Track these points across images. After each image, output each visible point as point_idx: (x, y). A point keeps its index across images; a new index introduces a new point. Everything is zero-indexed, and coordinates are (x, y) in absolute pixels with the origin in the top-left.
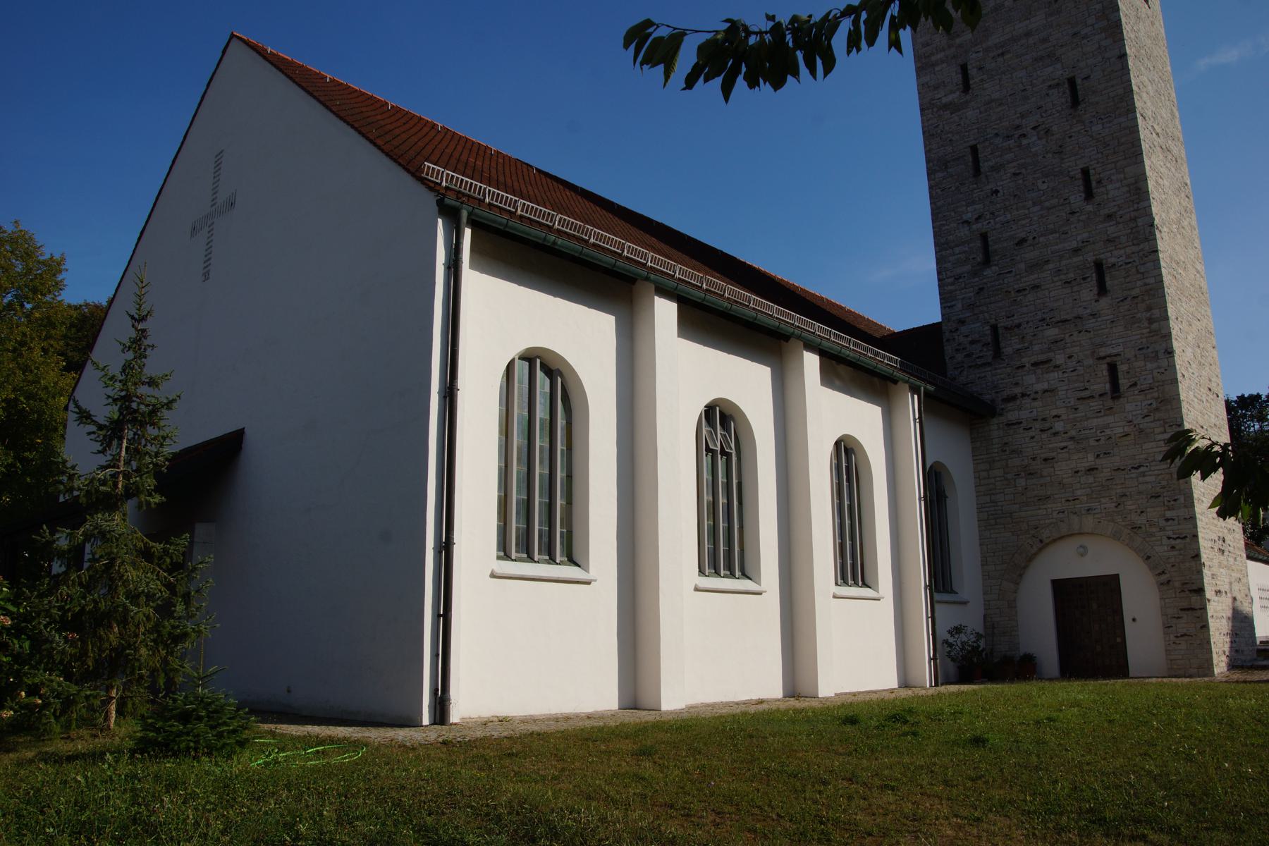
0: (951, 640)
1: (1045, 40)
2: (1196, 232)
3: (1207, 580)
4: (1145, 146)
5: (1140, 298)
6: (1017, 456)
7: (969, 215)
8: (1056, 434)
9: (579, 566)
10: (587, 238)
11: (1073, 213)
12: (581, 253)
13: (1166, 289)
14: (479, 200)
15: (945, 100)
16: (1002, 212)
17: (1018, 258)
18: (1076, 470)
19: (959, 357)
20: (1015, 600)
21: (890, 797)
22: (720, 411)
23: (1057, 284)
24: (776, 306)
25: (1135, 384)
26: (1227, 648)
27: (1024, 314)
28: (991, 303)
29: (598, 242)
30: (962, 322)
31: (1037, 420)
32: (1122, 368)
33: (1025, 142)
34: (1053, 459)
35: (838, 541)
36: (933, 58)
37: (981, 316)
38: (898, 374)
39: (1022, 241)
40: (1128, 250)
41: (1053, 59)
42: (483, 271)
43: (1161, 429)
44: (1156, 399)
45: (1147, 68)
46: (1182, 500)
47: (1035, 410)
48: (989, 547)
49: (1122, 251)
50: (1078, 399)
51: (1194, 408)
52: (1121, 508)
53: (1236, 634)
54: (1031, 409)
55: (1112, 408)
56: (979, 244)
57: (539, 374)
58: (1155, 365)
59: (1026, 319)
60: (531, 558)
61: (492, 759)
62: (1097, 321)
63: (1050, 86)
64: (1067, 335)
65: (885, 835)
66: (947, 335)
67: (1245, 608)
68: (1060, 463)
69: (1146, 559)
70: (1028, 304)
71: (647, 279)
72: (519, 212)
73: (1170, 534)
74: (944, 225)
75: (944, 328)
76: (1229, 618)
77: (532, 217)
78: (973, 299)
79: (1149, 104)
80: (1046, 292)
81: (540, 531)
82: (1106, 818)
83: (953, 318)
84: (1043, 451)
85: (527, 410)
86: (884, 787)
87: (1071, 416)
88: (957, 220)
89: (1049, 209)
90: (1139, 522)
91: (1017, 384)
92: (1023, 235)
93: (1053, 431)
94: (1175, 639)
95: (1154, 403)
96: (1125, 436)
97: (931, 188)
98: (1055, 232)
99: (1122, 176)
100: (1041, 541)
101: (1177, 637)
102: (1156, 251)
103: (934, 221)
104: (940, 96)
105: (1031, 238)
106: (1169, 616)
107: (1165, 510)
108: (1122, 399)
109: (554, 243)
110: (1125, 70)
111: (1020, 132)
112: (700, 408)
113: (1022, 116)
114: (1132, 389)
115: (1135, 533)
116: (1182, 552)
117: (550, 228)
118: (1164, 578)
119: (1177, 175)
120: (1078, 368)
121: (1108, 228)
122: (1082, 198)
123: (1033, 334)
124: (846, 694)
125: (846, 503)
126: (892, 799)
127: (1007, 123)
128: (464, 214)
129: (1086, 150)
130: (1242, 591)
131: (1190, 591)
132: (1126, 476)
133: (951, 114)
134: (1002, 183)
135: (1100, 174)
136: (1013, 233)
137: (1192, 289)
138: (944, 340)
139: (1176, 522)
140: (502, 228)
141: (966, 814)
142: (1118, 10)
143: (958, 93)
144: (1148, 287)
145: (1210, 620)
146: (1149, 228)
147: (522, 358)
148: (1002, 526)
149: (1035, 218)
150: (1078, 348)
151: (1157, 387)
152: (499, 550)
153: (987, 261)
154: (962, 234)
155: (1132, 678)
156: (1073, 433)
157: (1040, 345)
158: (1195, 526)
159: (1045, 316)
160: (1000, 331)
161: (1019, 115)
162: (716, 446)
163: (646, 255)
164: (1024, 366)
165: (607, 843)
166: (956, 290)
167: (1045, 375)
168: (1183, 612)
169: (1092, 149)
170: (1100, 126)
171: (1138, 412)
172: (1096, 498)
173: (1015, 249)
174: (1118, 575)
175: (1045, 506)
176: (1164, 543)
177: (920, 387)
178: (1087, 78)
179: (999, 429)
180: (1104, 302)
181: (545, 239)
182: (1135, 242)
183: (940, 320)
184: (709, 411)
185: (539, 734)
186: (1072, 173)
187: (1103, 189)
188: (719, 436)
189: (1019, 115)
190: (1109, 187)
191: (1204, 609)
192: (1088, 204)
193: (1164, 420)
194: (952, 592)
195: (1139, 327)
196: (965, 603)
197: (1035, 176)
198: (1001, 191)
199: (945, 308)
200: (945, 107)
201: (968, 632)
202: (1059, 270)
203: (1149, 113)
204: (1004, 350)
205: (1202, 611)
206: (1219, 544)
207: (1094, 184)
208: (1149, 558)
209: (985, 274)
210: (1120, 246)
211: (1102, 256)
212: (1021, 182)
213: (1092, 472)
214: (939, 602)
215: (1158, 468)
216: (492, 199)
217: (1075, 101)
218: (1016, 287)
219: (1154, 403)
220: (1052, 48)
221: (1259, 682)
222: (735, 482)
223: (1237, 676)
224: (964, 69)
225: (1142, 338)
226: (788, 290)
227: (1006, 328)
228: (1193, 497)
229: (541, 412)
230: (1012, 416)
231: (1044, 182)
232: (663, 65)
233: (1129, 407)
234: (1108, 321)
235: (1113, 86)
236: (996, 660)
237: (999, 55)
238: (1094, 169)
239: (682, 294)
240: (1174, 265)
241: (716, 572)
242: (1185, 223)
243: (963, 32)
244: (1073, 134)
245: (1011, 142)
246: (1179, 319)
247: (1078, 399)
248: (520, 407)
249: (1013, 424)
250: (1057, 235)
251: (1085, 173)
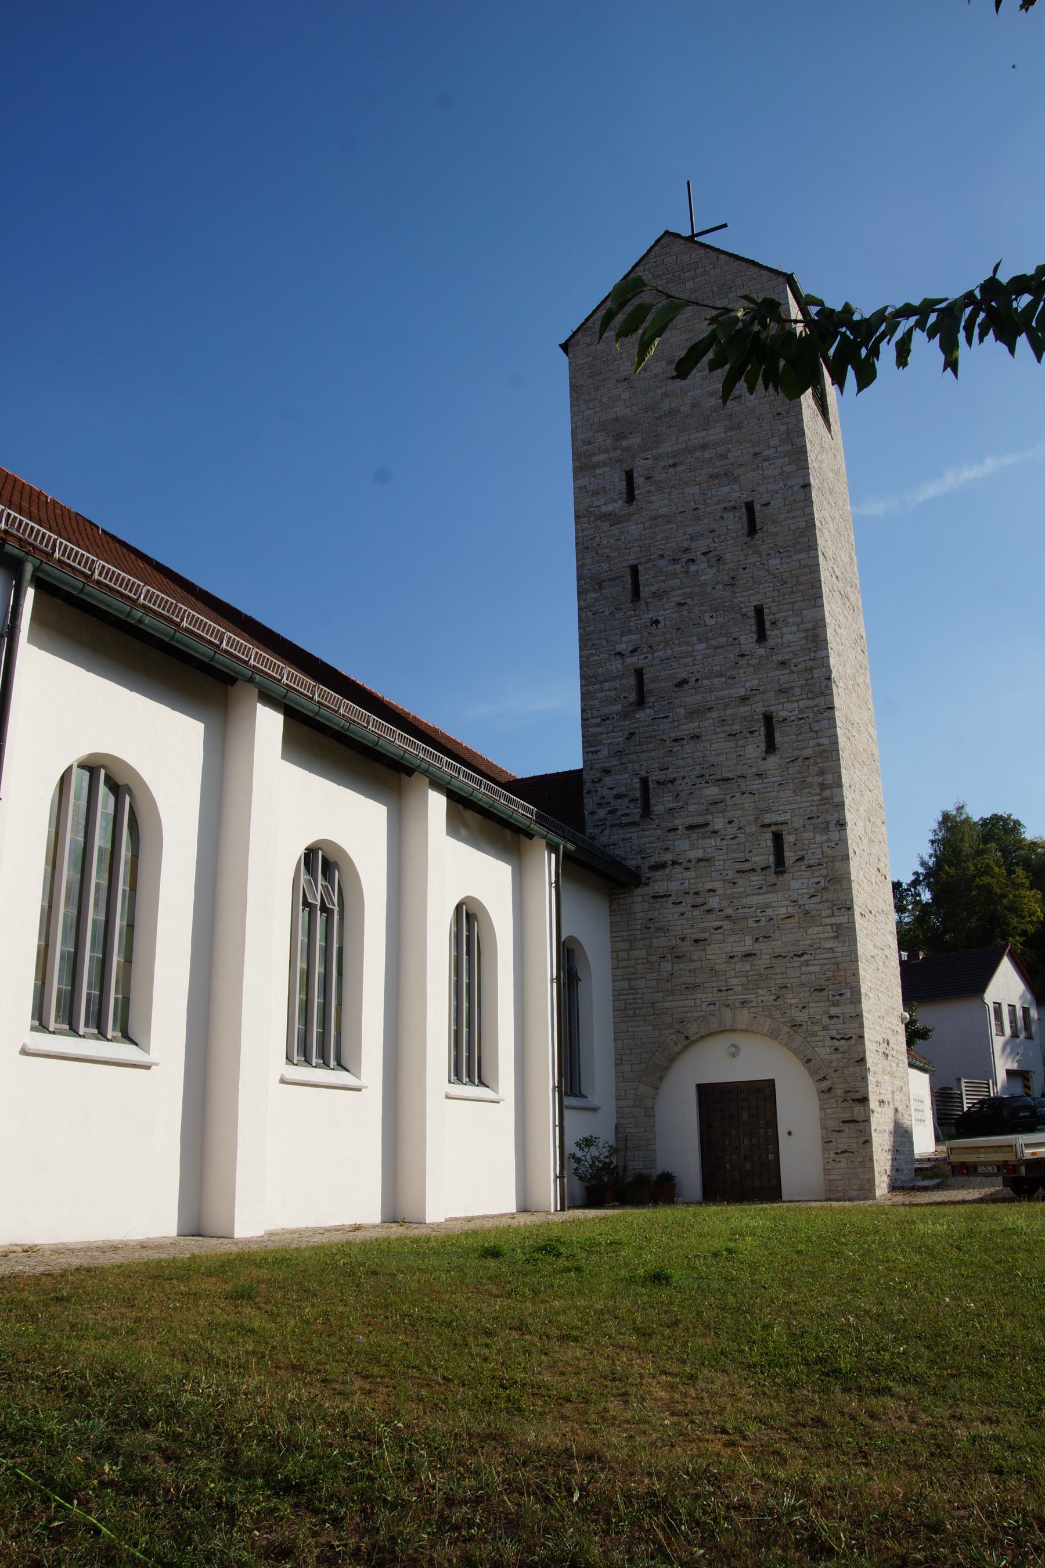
0: (579, 1154)
1: (723, 456)
2: (869, 692)
3: (871, 1088)
4: (825, 589)
5: (812, 760)
6: (663, 934)
7: (624, 646)
8: (710, 911)
9: (136, 1044)
10: (178, 620)
11: (742, 656)
12: (172, 638)
13: (841, 752)
14: (46, 553)
15: (605, 509)
16: (662, 646)
17: (677, 701)
18: (731, 955)
19: (602, 813)
20: (653, 1108)
21: (574, 1352)
22: (323, 856)
23: (721, 735)
24: (399, 731)
25: (802, 859)
26: (888, 1167)
27: (680, 768)
28: (642, 752)
29: (191, 627)
30: (607, 771)
31: (688, 893)
32: (789, 839)
33: (693, 568)
34: (706, 940)
35: (453, 1027)
36: (595, 459)
37: (630, 766)
38: (535, 827)
39: (684, 682)
40: (802, 704)
41: (731, 478)
42: (42, 647)
43: (829, 912)
44: (825, 877)
45: (829, 503)
46: (848, 995)
47: (687, 881)
48: (625, 1042)
49: (796, 704)
50: (738, 872)
51: (863, 889)
52: (780, 1001)
53: (897, 1151)
54: (682, 879)
55: (774, 884)
56: (632, 681)
57: (102, 789)
58: (825, 837)
59: (682, 774)
60: (74, 1031)
61: (35, 1306)
62: (762, 783)
63: (725, 508)
64: (728, 797)
65: (586, 1401)
66: (588, 786)
67: (905, 1121)
68: (712, 946)
69: (806, 1062)
70: (686, 756)
71: (251, 680)
72: (96, 576)
73: (834, 1033)
74: (592, 655)
75: (585, 776)
76: (891, 1132)
77: (112, 584)
78: (621, 746)
79: (830, 543)
80: (707, 744)
81: (89, 995)
82: (841, 1370)
83: (597, 766)
84: (693, 930)
85: (82, 834)
86: (564, 1338)
87: (728, 892)
88: (610, 650)
89: (716, 648)
90: (800, 1019)
91: (667, 849)
92: (684, 676)
93: (707, 907)
94: (835, 1155)
95: (822, 882)
96: (789, 917)
97: (580, 609)
98: (721, 675)
99: (799, 619)
100: (687, 1038)
101: (837, 1153)
102: (832, 708)
103: (581, 649)
104: (598, 504)
105: (693, 679)
106: (829, 1129)
107: (828, 1007)
108: (786, 875)
109: (140, 621)
110: (808, 501)
111: (689, 556)
112: (301, 851)
113: (692, 538)
114: (798, 864)
115: (794, 1031)
116: (846, 1055)
117: (134, 602)
118: (825, 1085)
119: (854, 625)
120: (739, 835)
121: (781, 677)
122: (754, 640)
123: (689, 792)
124: (457, 1219)
125: (465, 980)
126: (579, 1353)
127: (675, 544)
128: (29, 569)
129: (761, 586)
130: (904, 1101)
131: (853, 1100)
132: (788, 965)
133: (611, 526)
134: (664, 613)
135: (774, 614)
136: (672, 671)
137: (865, 755)
138: (585, 791)
139: (841, 1020)
140: (75, 592)
141: (674, 1369)
142: (804, 435)
143: (620, 502)
144: (822, 748)
145: (874, 1134)
146: (826, 681)
147: (82, 766)
148: (643, 1018)
149: (700, 657)
150: (740, 812)
151: (827, 863)
152: (33, 1018)
153: (641, 702)
154: (614, 667)
155: (785, 1202)
156: (729, 911)
157: (696, 806)
158: (862, 1026)
159: (703, 772)
160: (651, 785)
161: (688, 536)
162: (315, 899)
163: (248, 651)
164: (677, 829)
165: (251, 1424)
166: (602, 733)
167: (701, 841)
168: (845, 1124)
169: (768, 585)
170: (778, 561)
171: (805, 891)
172: (753, 989)
173: (674, 691)
174: (773, 1081)
175: (694, 996)
176: (827, 1044)
177: (558, 845)
178: (767, 504)
179: (643, 901)
180: (773, 761)
181: (129, 615)
182: (810, 695)
183: (579, 765)
184: (310, 854)
185: (89, 1270)
186: (744, 610)
187: (777, 632)
188: (320, 887)
189: (688, 536)
190: (785, 630)
191: (867, 1121)
192: (760, 647)
193: (832, 901)
194: (581, 1095)
195: (809, 792)
196: (594, 1110)
197: (704, 608)
198: (662, 622)
199: (587, 752)
200: (604, 517)
201: (600, 1145)
202: (724, 720)
203: (829, 553)
204: (654, 808)
205: (865, 1124)
206: (883, 1048)
207: (768, 625)
208: (809, 1061)
209: (637, 716)
210: (793, 698)
211: (772, 708)
212: (685, 613)
213: (750, 959)
214: (567, 1107)
215: (822, 956)
216: (63, 555)
217: (752, 530)
218: (673, 735)
219: (822, 882)
220: (730, 466)
221: (927, 1204)
222: (335, 946)
223: (900, 1198)
224: (629, 476)
225: (812, 806)
226: (398, 715)
227: (659, 783)
228: (859, 991)
229: (101, 840)
230: (660, 887)
231: (712, 617)
232: (1032, 298)
233: (794, 885)
234: (776, 784)
235: (794, 518)
236: (630, 1179)
237: (670, 466)
238: (769, 608)
239: (291, 704)
240: (849, 726)
241: (306, 1061)
242: (860, 680)
243: (631, 433)
244: (748, 566)
245: (677, 566)
246: (852, 787)
247: (738, 872)
248: (75, 830)
249: (660, 897)
250: (723, 679)
251: (759, 611)
